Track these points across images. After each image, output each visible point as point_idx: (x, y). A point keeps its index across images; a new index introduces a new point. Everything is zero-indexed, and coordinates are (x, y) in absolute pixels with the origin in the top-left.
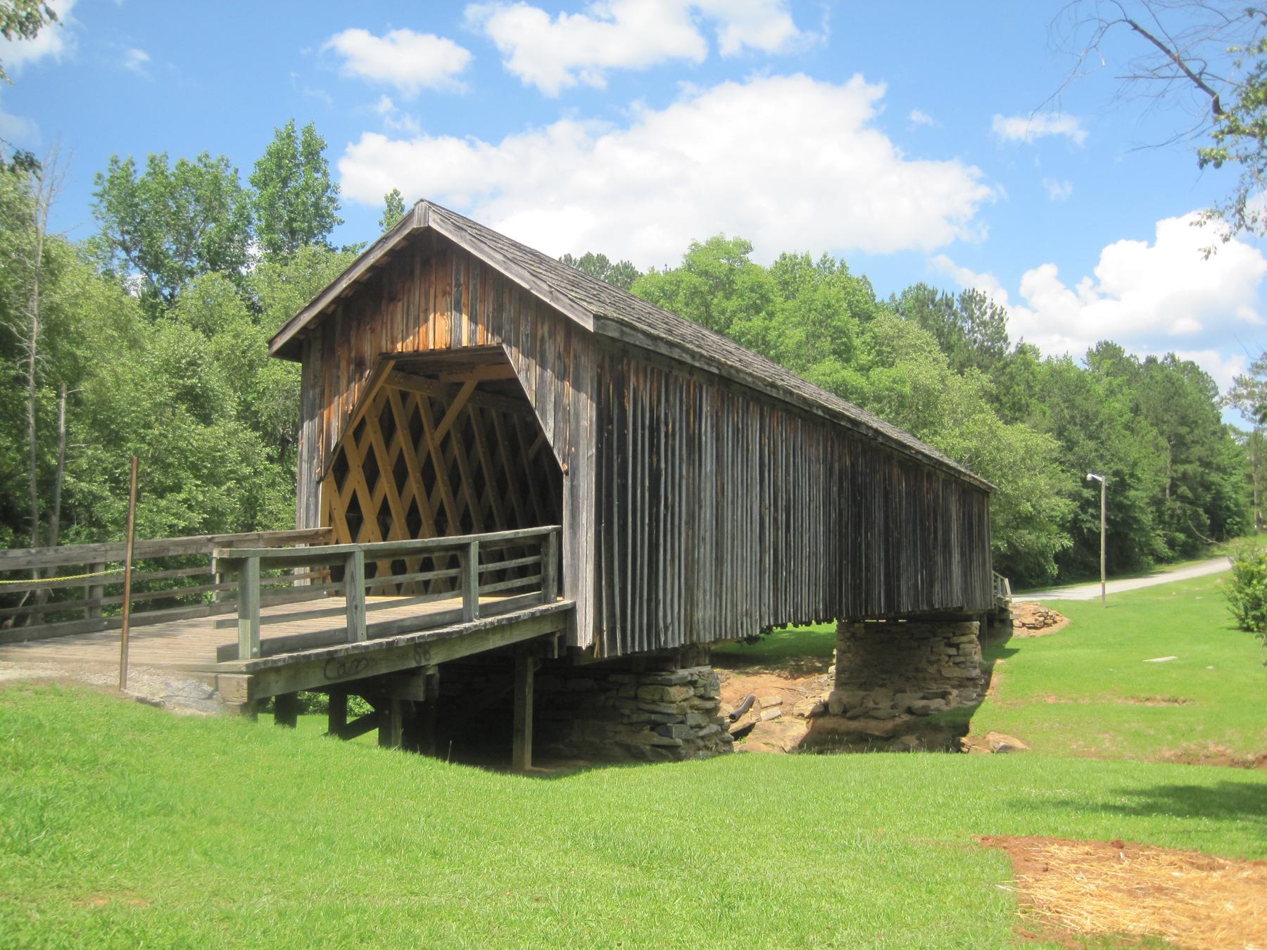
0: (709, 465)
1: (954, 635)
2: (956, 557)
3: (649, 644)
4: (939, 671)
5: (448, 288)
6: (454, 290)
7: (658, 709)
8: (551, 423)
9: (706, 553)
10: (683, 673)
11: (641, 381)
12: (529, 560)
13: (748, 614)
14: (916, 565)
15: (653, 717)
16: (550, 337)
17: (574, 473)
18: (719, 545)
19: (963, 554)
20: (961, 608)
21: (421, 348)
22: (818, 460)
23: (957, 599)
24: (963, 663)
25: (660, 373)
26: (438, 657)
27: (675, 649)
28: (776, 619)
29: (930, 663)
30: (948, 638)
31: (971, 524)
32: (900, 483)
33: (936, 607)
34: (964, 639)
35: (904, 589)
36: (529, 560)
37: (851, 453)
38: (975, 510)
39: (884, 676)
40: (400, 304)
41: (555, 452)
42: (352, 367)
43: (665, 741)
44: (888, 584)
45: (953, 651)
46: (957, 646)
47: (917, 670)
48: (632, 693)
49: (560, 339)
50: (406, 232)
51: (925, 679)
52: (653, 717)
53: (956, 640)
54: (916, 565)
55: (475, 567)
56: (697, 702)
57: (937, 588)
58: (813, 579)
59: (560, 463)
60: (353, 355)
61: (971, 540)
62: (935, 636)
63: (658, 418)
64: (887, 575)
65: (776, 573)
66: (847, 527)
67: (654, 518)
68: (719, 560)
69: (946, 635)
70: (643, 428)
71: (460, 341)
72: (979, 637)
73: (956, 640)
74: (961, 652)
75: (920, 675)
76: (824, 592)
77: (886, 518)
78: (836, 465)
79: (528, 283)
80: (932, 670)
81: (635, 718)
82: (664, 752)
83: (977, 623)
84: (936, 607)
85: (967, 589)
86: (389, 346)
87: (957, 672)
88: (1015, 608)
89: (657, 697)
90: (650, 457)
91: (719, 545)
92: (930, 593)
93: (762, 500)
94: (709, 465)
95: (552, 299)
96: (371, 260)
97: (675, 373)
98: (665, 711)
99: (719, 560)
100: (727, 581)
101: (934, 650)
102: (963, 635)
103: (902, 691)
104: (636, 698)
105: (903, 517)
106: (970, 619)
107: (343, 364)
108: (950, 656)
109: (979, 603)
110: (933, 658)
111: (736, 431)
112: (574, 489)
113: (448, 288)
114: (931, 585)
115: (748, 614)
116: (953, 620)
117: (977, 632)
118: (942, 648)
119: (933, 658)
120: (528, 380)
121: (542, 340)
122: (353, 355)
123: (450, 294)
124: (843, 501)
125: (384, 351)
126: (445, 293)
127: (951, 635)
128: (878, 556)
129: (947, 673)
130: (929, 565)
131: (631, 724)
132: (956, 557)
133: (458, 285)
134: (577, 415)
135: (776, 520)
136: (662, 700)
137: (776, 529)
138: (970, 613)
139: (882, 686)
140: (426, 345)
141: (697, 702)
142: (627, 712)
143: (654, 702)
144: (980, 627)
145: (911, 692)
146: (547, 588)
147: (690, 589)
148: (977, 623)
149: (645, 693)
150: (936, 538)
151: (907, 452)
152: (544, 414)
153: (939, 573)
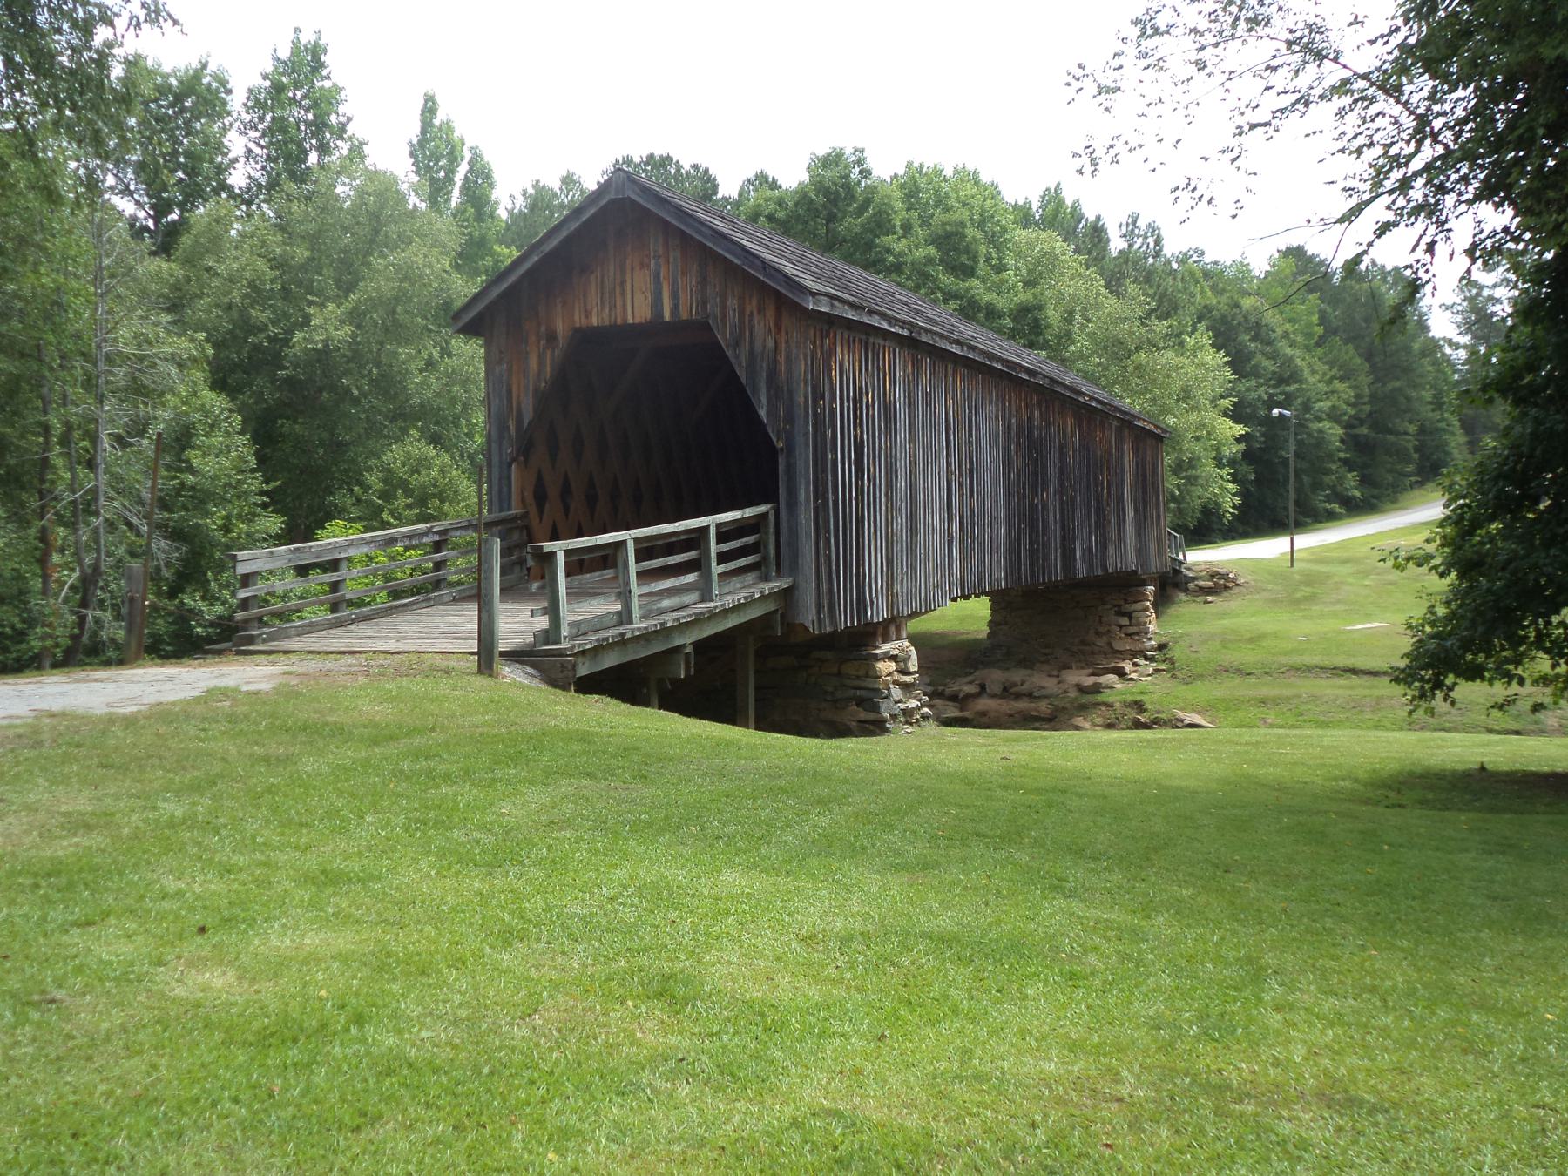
0: (902, 436)
1: (1126, 601)
2: (1130, 513)
3: (859, 620)
4: (1110, 644)
5: (646, 260)
6: (653, 262)
7: (863, 684)
8: (764, 400)
9: (902, 522)
10: (885, 647)
11: (846, 352)
12: (750, 539)
13: (939, 586)
14: (1090, 526)
15: (859, 693)
16: (759, 311)
17: (790, 449)
18: (913, 516)
19: (1136, 510)
20: (1135, 572)
21: (619, 321)
22: (997, 418)
23: (1131, 562)
24: (1137, 634)
25: (861, 340)
26: (687, 639)
27: (879, 623)
28: (963, 590)
29: (1098, 634)
30: (1119, 606)
31: (1144, 476)
32: (1074, 435)
33: (1110, 571)
34: (1138, 606)
35: (1078, 553)
36: (750, 539)
37: (1027, 406)
38: (1149, 458)
39: (1047, 651)
40: (593, 278)
41: (770, 431)
42: (543, 342)
43: (871, 716)
44: (1063, 546)
45: (1124, 621)
46: (1129, 615)
47: (1083, 643)
48: (835, 670)
49: (770, 313)
50: (604, 202)
51: (1093, 653)
52: (859, 693)
53: (1129, 607)
54: (1090, 526)
55: (714, 548)
56: (897, 676)
57: (1111, 551)
58: (995, 546)
59: (775, 440)
60: (543, 329)
61: (1145, 492)
62: (1104, 604)
63: (861, 388)
64: (1063, 538)
65: (962, 541)
66: (1024, 488)
67: (860, 490)
68: (914, 531)
69: (1116, 603)
70: (848, 401)
71: (662, 317)
72: (1154, 605)
73: (1129, 607)
74: (1134, 621)
75: (1087, 648)
76: (1005, 558)
77: (1061, 473)
78: (1013, 421)
79: (739, 258)
80: (1101, 642)
81: (839, 694)
82: (871, 727)
83: (1151, 588)
84: (1110, 571)
85: (1141, 551)
86: (583, 320)
87: (1128, 645)
88: (1189, 569)
89: (861, 673)
90: (855, 430)
91: (913, 516)
92: (1104, 554)
93: (948, 464)
94: (902, 436)
95: (765, 276)
96: (564, 233)
97: (871, 340)
98: (871, 686)
99: (914, 531)
100: (921, 551)
101: (1104, 619)
102: (1135, 602)
103: (1067, 667)
104: (839, 674)
105: (1078, 473)
106: (1144, 583)
107: (533, 339)
108: (1121, 627)
109: (1155, 566)
110: (1102, 629)
111: (925, 394)
112: (791, 468)
113: (646, 260)
114: (1105, 547)
115: (939, 586)
116: (1124, 587)
117: (1151, 598)
118: (1114, 618)
119: (1102, 629)
120: (737, 357)
121: (751, 314)
122: (543, 329)
123: (648, 266)
124: (1020, 460)
125: (578, 325)
126: (642, 266)
127: (1122, 602)
128: (1054, 516)
129: (1118, 646)
130: (1102, 525)
131: (835, 701)
132: (1130, 513)
133: (657, 257)
134: (790, 392)
135: (961, 485)
136: (867, 676)
137: (961, 495)
138: (1144, 577)
139: (1047, 662)
140: (625, 319)
141: (897, 676)
142: (830, 689)
143: (858, 677)
144: (1155, 592)
145: (1077, 668)
146: (767, 567)
147: (890, 562)
148: (1151, 588)
149: (849, 669)
150: (1109, 493)
151: (1081, 399)
152: (755, 390)
153: (1113, 534)
